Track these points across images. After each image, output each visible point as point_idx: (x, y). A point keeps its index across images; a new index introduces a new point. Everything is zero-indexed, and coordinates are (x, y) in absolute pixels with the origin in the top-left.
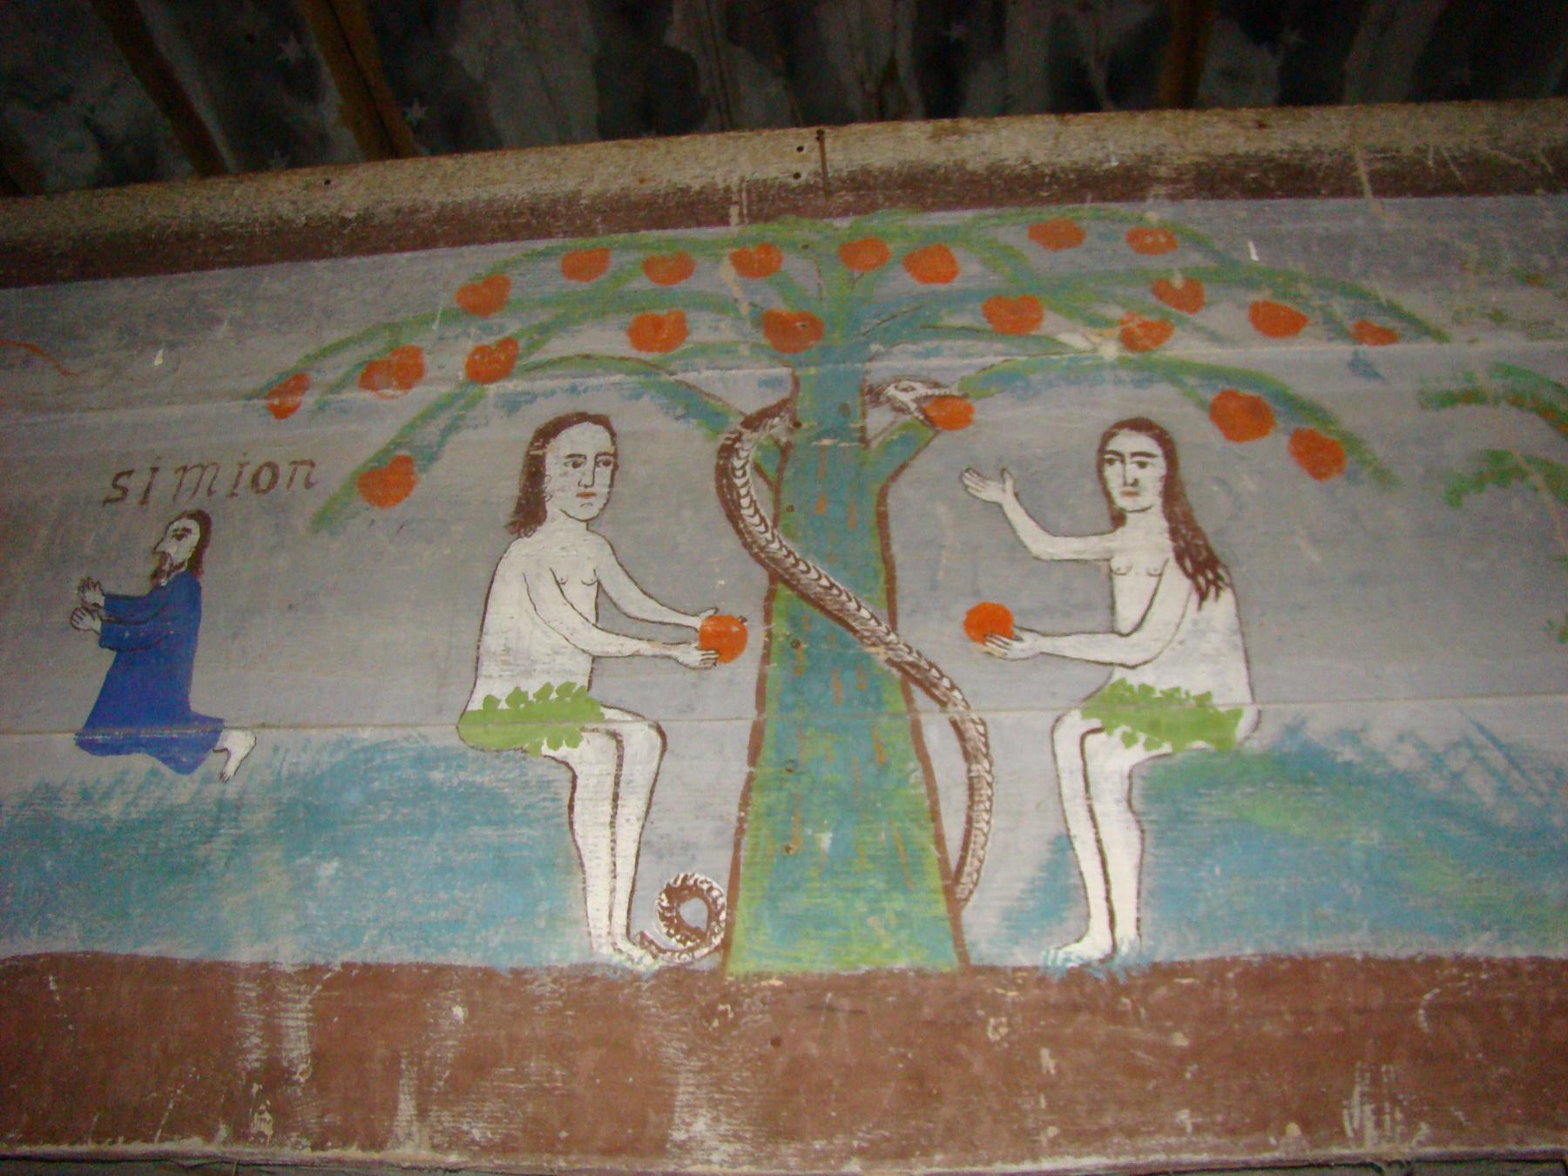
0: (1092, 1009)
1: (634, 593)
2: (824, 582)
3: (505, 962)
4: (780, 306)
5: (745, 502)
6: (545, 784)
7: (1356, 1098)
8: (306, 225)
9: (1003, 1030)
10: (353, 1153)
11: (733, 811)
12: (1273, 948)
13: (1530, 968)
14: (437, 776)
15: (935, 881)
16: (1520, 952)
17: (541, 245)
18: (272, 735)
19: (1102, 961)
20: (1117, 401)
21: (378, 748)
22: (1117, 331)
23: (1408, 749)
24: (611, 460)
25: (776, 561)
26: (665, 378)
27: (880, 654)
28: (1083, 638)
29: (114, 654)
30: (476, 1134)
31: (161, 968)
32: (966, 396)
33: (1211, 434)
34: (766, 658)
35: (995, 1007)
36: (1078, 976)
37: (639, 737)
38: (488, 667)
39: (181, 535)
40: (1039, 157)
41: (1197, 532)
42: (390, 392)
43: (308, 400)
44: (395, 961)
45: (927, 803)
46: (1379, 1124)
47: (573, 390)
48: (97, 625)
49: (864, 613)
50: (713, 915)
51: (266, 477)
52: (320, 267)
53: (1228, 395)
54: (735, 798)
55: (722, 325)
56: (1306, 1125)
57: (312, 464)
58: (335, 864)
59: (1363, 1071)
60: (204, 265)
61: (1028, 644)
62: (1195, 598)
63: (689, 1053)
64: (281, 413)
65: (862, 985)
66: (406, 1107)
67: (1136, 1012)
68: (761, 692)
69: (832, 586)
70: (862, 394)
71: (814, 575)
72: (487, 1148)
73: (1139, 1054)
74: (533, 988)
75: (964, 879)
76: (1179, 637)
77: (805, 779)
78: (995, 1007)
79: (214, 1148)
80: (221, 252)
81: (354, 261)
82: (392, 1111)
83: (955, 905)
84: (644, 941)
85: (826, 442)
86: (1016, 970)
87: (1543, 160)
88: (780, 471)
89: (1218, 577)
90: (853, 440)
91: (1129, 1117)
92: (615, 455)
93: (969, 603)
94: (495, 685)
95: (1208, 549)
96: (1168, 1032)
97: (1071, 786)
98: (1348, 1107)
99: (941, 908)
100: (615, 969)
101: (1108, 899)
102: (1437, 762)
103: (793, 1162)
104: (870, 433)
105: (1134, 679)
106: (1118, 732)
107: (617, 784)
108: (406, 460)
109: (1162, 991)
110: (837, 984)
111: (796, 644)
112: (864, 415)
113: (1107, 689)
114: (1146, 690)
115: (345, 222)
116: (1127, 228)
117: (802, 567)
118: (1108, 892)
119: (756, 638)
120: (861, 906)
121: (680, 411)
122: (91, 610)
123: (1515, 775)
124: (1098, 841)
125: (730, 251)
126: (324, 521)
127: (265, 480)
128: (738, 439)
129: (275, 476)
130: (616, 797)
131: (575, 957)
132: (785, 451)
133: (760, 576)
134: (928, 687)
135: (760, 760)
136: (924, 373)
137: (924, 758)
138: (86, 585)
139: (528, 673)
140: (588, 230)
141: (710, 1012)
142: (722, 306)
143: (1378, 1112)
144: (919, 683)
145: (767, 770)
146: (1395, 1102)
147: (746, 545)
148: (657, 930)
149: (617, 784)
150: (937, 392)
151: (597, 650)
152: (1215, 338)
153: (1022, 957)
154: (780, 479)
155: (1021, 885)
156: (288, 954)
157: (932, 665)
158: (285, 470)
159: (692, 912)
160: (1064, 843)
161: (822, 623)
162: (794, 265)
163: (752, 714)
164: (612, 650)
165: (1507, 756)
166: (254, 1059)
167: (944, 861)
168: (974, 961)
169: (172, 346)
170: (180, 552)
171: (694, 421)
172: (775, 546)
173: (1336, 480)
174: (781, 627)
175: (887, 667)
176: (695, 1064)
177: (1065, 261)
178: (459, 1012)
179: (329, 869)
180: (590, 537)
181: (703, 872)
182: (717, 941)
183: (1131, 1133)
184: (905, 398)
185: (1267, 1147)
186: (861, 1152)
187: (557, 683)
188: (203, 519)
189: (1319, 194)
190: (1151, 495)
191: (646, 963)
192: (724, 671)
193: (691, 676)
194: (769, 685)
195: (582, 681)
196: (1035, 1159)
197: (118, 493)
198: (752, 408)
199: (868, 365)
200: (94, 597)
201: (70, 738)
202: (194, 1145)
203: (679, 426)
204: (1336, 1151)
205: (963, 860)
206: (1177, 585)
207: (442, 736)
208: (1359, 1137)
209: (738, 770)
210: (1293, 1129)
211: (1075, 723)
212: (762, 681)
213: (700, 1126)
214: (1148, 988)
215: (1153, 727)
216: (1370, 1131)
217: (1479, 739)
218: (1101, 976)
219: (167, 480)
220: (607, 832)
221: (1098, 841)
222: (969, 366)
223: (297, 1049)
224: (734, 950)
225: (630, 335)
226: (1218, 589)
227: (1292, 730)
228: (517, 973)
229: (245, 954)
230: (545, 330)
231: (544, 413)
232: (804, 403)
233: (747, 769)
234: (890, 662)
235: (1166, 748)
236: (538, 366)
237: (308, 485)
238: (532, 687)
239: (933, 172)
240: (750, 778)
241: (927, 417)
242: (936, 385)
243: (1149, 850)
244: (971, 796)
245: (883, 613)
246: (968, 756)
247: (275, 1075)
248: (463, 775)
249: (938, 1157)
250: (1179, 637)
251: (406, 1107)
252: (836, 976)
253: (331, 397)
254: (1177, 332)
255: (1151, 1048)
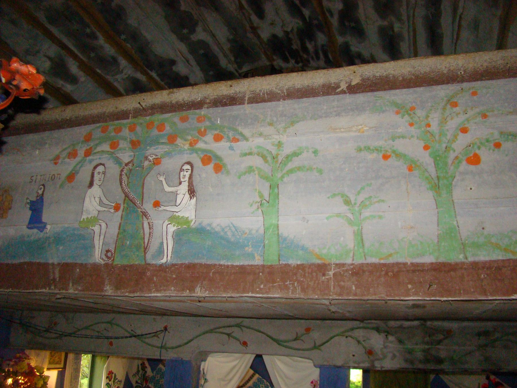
0: (162, 271)
1: (105, 199)
2: (133, 197)
3: (84, 262)
4: (134, 139)
5: (123, 181)
6: (90, 234)
7: (198, 286)
8: (61, 121)
9: (150, 274)
10: (64, 291)
11: (116, 238)
12: (191, 262)
13: (230, 266)
14: (76, 232)
15: (143, 250)
16: (229, 264)
17: (98, 125)
18: (53, 225)
19: (165, 263)
20: (186, 158)
21: (68, 228)
22: (189, 142)
23: (218, 227)
24: (104, 173)
25: (126, 193)
26: (114, 155)
27: (140, 210)
28: (170, 207)
29: (31, 211)
30: (79, 288)
31: (39, 264)
32: (161, 158)
33: (201, 164)
34: (123, 211)
35: (149, 270)
36: (161, 265)
37: (104, 225)
38: (84, 213)
39: (41, 189)
40: (186, 99)
41: (193, 185)
42: (72, 159)
43: (60, 161)
44: (70, 262)
45: (143, 236)
46: (201, 291)
47: (100, 158)
48: (29, 206)
49: (138, 203)
50: (112, 255)
51: (53, 177)
52: (62, 130)
53: (205, 156)
54: (116, 235)
55: (125, 143)
56: (190, 291)
57: (60, 174)
58: (62, 247)
59: (200, 282)
60: (44, 130)
61: (162, 208)
62: (190, 199)
63: (107, 276)
64: (56, 164)
65: (131, 266)
66: (71, 285)
67: (168, 272)
68: (122, 217)
69: (134, 197)
70: (145, 158)
71: (131, 195)
72: (80, 291)
73: (168, 278)
74: (88, 266)
75: (147, 249)
76: (186, 206)
77: (126, 232)
78: (149, 270)
79: (46, 291)
80: (47, 128)
81: (68, 129)
82: (69, 285)
83: (145, 253)
84: (103, 259)
85: (137, 168)
86: (153, 264)
87: (285, 91)
88: (129, 175)
89: (194, 195)
90: (141, 168)
91: (165, 288)
92: (105, 172)
93: (154, 200)
94: (84, 217)
95: (194, 189)
96: (172, 275)
97: (165, 233)
98: (197, 288)
99: (143, 254)
100: (99, 263)
101: (167, 253)
102: (223, 229)
103: (119, 293)
104: (145, 166)
105: (177, 214)
106: (173, 224)
107: (100, 233)
108: (74, 174)
109: (173, 268)
110: (127, 266)
111: (128, 208)
112: (144, 163)
113: (172, 216)
114: (179, 216)
115: (67, 120)
116: (197, 116)
117: (130, 194)
118: (167, 252)
119: (122, 208)
120: (132, 253)
121: (116, 163)
122: (28, 203)
123: (236, 232)
124: (167, 243)
125: (128, 125)
126: (62, 186)
127: (53, 178)
128: (124, 168)
129: (55, 177)
130: (100, 236)
131: (93, 262)
132: (131, 170)
133: (123, 196)
134: (146, 216)
135: (120, 229)
136: (155, 153)
137: (143, 229)
138: (27, 199)
139: (89, 214)
140: (106, 121)
141: (111, 270)
142: (125, 139)
143: (201, 289)
144: (144, 215)
145: (121, 231)
146: (204, 287)
147: (122, 190)
148: (104, 257)
149: (100, 233)
150: (156, 157)
151: (99, 210)
152: (206, 143)
153: (154, 262)
154: (129, 177)
155: (155, 250)
156: (56, 261)
157: (147, 212)
158: (56, 175)
159: (109, 254)
160: (162, 243)
161: (132, 204)
162: (138, 129)
163: (120, 221)
164: (101, 210)
165: (235, 229)
166: (52, 277)
167: (144, 246)
168: (147, 263)
169: (39, 149)
170: (40, 192)
171: (117, 165)
172: (127, 190)
173: (220, 174)
174: (126, 205)
175: (140, 212)
176: (108, 278)
177: (185, 125)
178: (78, 270)
179: (61, 248)
180: (100, 189)
181: (111, 248)
182: (112, 259)
183: (165, 290)
184: (151, 158)
185: (183, 293)
186: (128, 292)
187: (93, 216)
188: (43, 185)
189: (236, 104)
190: (187, 179)
191: (103, 262)
192: (117, 213)
193: (112, 214)
194: (123, 216)
195: (96, 215)
196: (151, 294)
197: (31, 181)
198: (127, 162)
199: (146, 152)
200: (28, 201)
201: (25, 227)
202: (44, 290)
203: (115, 166)
204: (193, 295)
205: (147, 246)
206: (187, 196)
207: (76, 225)
208: (197, 293)
209: (117, 231)
210: (188, 291)
211: (167, 222)
212: (122, 215)
213: (108, 288)
214: (171, 268)
215: (178, 223)
216: (199, 292)
217: (231, 225)
218: (164, 265)
219: (39, 177)
220: (98, 241)
221: (167, 243)
222: (162, 151)
223: (57, 276)
224: (114, 260)
225: (110, 146)
226: (194, 197)
227: (200, 224)
228: (86, 264)
229: (51, 261)
230: (97, 145)
231: (95, 163)
232: (135, 161)
233: (118, 231)
234: (141, 212)
235: (180, 227)
236: (95, 153)
237: (60, 179)
238: (90, 216)
239: (166, 104)
240: (119, 232)
241: (154, 163)
242: (157, 156)
243: (174, 245)
244: (150, 235)
245: (141, 203)
246: (150, 228)
247: (54, 279)
248: (79, 232)
249: (138, 293)
250: (186, 206)
251: (71, 285)
252: (128, 265)
253: (64, 161)
254: (200, 142)
255: (170, 277)
